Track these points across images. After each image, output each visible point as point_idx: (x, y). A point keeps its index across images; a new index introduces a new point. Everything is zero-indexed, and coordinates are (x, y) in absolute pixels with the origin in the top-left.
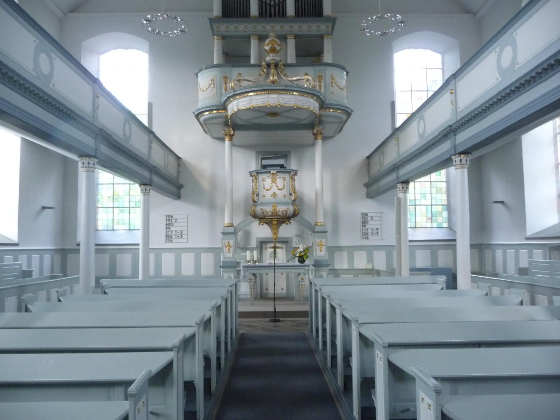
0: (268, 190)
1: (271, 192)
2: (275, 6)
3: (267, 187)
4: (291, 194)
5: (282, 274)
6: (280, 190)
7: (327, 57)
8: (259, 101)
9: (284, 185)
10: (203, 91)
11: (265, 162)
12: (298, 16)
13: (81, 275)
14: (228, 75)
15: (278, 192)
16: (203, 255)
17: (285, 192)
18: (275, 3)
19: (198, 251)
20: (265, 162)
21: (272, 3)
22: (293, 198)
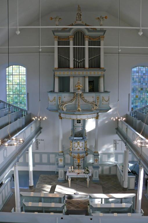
0: (77, 147)
1: (77, 149)
2: (82, 62)
3: (76, 147)
4: (85, 149)
5: (76, 162)
6: (81, 147)
7: (102, 89)
8: (120, 178)
9: (82, 145)
10: (51, 101)
11: (103, 200)
12: (75, 68)
13: (10, 171)
14: (61, 97)
15: (80, 148)
16: (51, 155)
17: (83, 148)
18: (80, 61)
19: (48, 154)
20: (103, 200)
21: (79, 61)
22: (85, 150)
